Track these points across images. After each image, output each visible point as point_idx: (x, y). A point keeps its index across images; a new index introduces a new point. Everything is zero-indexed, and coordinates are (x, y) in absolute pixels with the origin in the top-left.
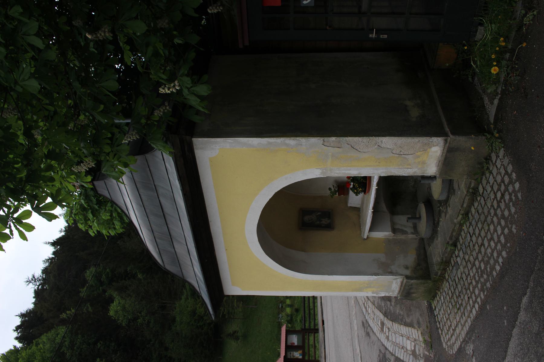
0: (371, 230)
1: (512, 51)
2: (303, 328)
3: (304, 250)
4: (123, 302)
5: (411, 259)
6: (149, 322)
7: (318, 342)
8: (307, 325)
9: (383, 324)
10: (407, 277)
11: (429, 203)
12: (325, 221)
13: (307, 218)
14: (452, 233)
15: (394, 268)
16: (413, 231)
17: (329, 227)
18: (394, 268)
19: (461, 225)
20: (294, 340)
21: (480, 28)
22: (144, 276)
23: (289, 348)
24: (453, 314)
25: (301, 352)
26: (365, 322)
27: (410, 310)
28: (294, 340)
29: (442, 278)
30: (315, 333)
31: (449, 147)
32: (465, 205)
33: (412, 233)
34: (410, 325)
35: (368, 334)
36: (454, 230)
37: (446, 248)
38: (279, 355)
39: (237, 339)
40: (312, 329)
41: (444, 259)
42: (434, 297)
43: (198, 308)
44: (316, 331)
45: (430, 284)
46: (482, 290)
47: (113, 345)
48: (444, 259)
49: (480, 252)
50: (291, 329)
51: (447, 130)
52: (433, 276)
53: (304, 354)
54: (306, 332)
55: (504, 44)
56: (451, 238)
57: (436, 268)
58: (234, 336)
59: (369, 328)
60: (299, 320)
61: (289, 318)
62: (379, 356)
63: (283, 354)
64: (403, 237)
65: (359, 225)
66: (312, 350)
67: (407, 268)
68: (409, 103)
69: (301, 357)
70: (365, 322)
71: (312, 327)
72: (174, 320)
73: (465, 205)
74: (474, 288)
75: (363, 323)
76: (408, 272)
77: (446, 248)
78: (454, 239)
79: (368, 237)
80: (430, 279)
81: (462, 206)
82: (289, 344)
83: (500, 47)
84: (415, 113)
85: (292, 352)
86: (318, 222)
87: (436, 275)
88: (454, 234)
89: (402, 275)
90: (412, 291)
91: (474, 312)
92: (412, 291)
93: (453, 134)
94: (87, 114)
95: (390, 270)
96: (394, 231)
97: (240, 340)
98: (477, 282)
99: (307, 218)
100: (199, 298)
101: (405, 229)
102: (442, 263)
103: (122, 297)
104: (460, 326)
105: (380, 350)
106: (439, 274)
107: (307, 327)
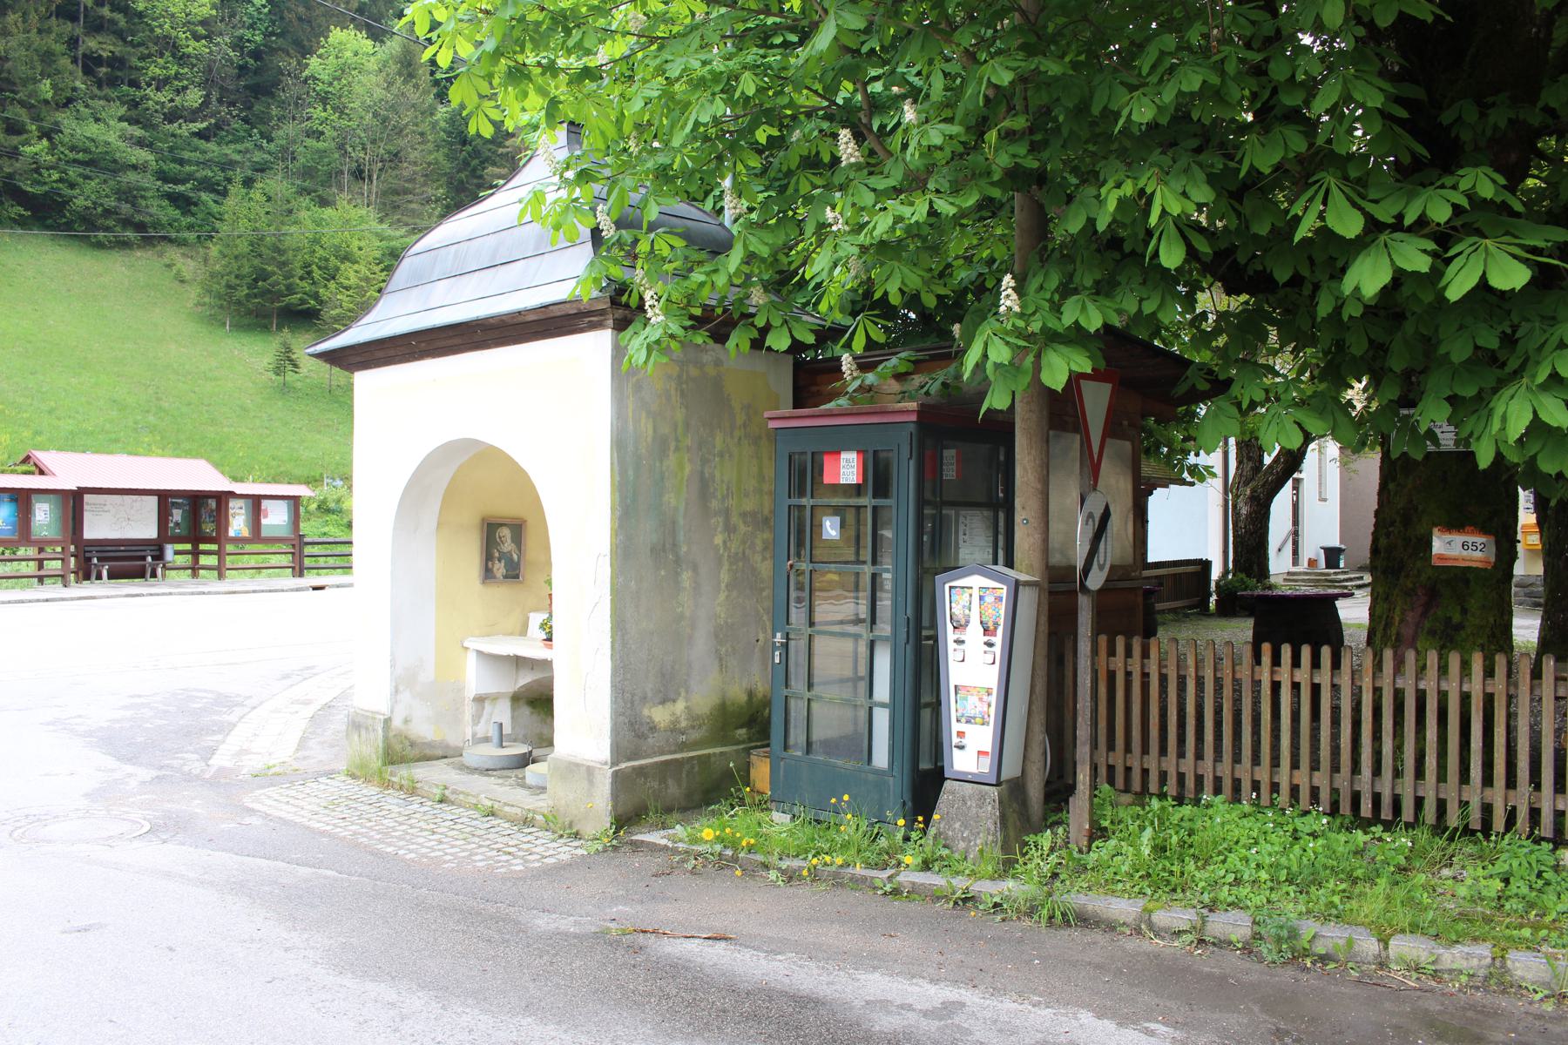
0: (480, 653)
1: (735, 859)
2: (307, 540)
3: (439, 525)
4: (372, 65)
5: (424, 730)
6: (319, 135)
7: (269, 576)
8: (316, 550)
9: (307, 703)
10: (387, 722)
11: (525, 761)
12: (499, 568)
13: (505, 532)
14: (462, 793)
15: (406, 697)
16: (479, 736)
17: (488, 574)
18: (406, 697)
19: (475, 807)
20: (276, 518)
21: (789, 817)
22: (443, 124)
23: (256, 502)
24: (318, 801)
25: (246, 533)
26: (314, 671)
27: (332, 746)
28: (276, 518)
29: (387, 785)
30: (293, 568)
31: (594, 768)
32: (507, 809)
33: (474, 735)
34: (302, 743)
35: (286, 677)
36: (468, 795)
37: (437, 786)
38: (235, 479)
39: (278, 371)
40: (301, 551)
41: (418, 785)
42: (353, 776)
43: (356, 267)
44: (299, 570)
45: (376, 763)
46: (355, 833)
47: (257, 38)
48: (418, 785)
49: (422, 830)
50: (302, 509)
51: (623, 766)
52: (390, 768)
53: (238, 540)
54: (294, 546)
55: (744, 843)
56: (454, 792)
57: (402, 773)
58: (287, 361)
59: (300, 678)
60: (326, 529)
61: (332, 505)
62: (238, 695)
63: (239, 488)
64: (468, 716)
65: (490, 631)
66: (252, 561)
67: (406, 721)
68: (680, 706)
69: (232, 533)
70: (314, 671)
71: (307, 562)
72: (324, 202)
73: (507, 809)
74: (361, 825)
75: (312, 668)
76: (397, 723)
77: (437, 786)
78: (452, 797)
79: (467, 648)
80: (385, 764)
81: (505, 804)
82: (265, 504)
83: (741, 839)
84: (660, 715)
85: (243, 511)
86: (497, 555)
87: (392, 774)
88: (461, 797)
89: (392, 712)
90: (363, 732)
91: (317, 825)
92: (363, 732)
93: (616, 775)
94: (778, 40)
95: (401, 688)
96: (480, 700)
97: (274, 377)
98: (370, 828)
99: (505, 532)
100: (382, 271)
101: (483, 720)
102: (413, 781)
103: (385, 66)
104: (294, 809)
105: (250, 697)
106: (393, 779)
107: (308, 550)
